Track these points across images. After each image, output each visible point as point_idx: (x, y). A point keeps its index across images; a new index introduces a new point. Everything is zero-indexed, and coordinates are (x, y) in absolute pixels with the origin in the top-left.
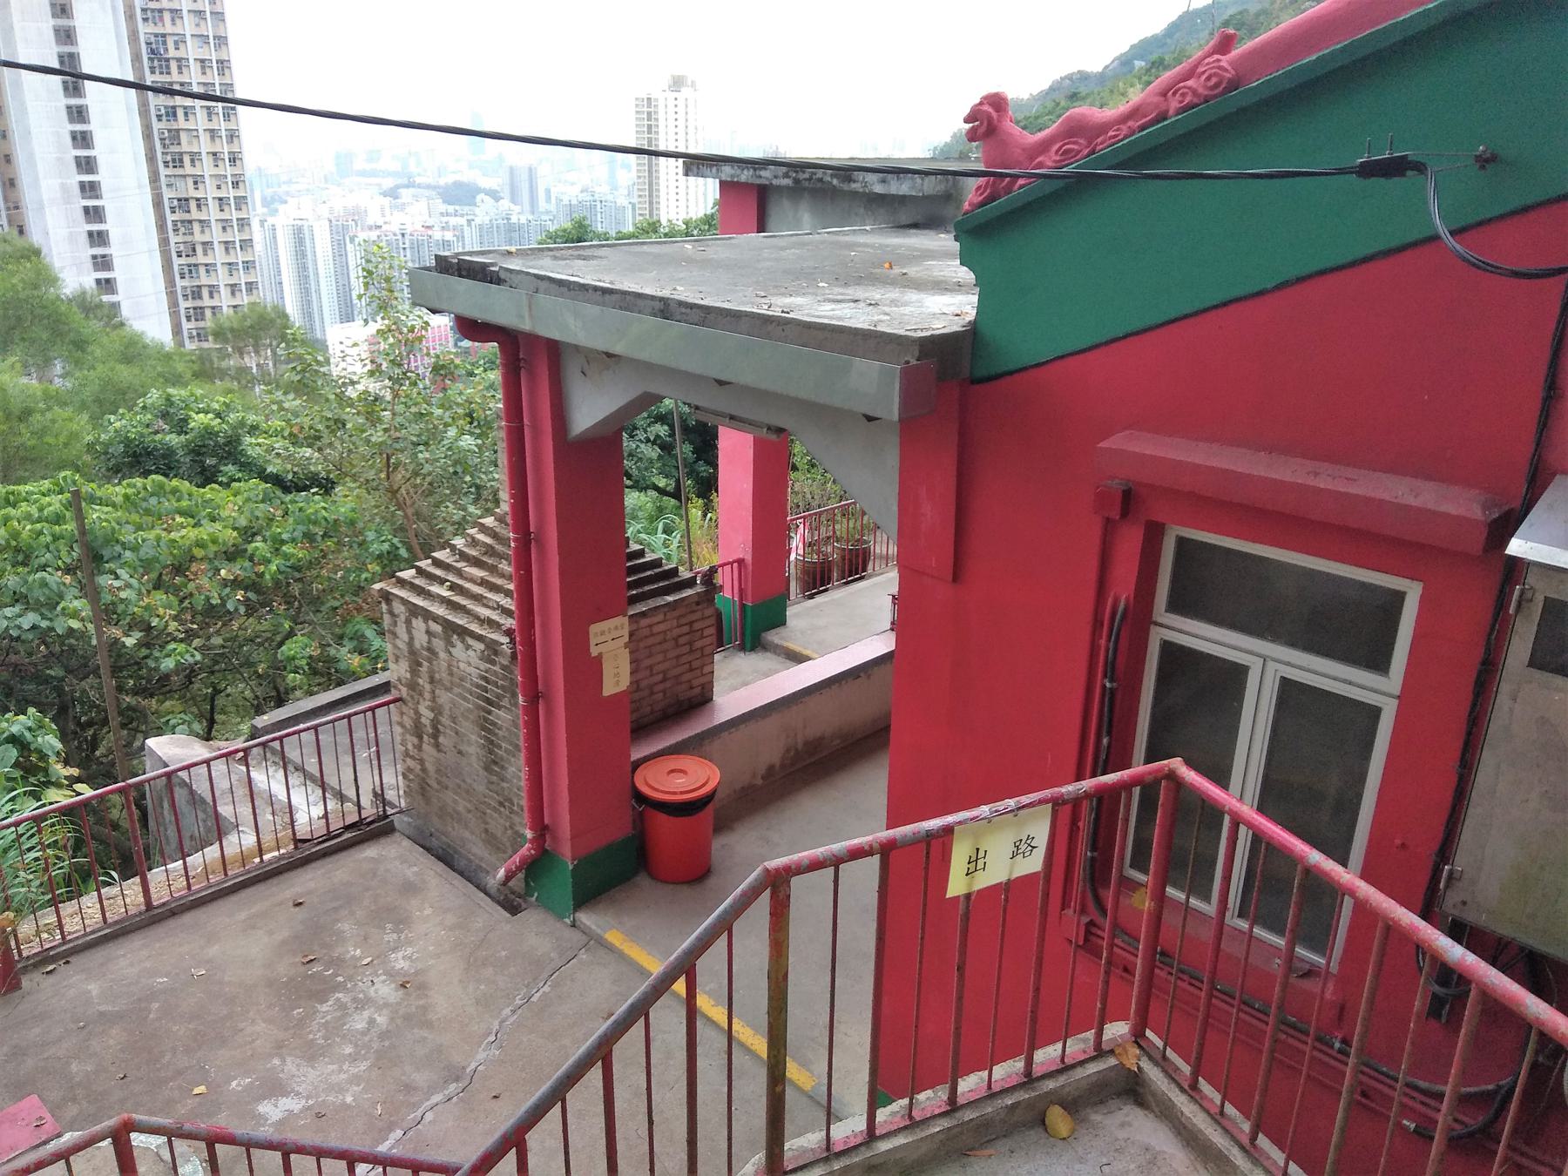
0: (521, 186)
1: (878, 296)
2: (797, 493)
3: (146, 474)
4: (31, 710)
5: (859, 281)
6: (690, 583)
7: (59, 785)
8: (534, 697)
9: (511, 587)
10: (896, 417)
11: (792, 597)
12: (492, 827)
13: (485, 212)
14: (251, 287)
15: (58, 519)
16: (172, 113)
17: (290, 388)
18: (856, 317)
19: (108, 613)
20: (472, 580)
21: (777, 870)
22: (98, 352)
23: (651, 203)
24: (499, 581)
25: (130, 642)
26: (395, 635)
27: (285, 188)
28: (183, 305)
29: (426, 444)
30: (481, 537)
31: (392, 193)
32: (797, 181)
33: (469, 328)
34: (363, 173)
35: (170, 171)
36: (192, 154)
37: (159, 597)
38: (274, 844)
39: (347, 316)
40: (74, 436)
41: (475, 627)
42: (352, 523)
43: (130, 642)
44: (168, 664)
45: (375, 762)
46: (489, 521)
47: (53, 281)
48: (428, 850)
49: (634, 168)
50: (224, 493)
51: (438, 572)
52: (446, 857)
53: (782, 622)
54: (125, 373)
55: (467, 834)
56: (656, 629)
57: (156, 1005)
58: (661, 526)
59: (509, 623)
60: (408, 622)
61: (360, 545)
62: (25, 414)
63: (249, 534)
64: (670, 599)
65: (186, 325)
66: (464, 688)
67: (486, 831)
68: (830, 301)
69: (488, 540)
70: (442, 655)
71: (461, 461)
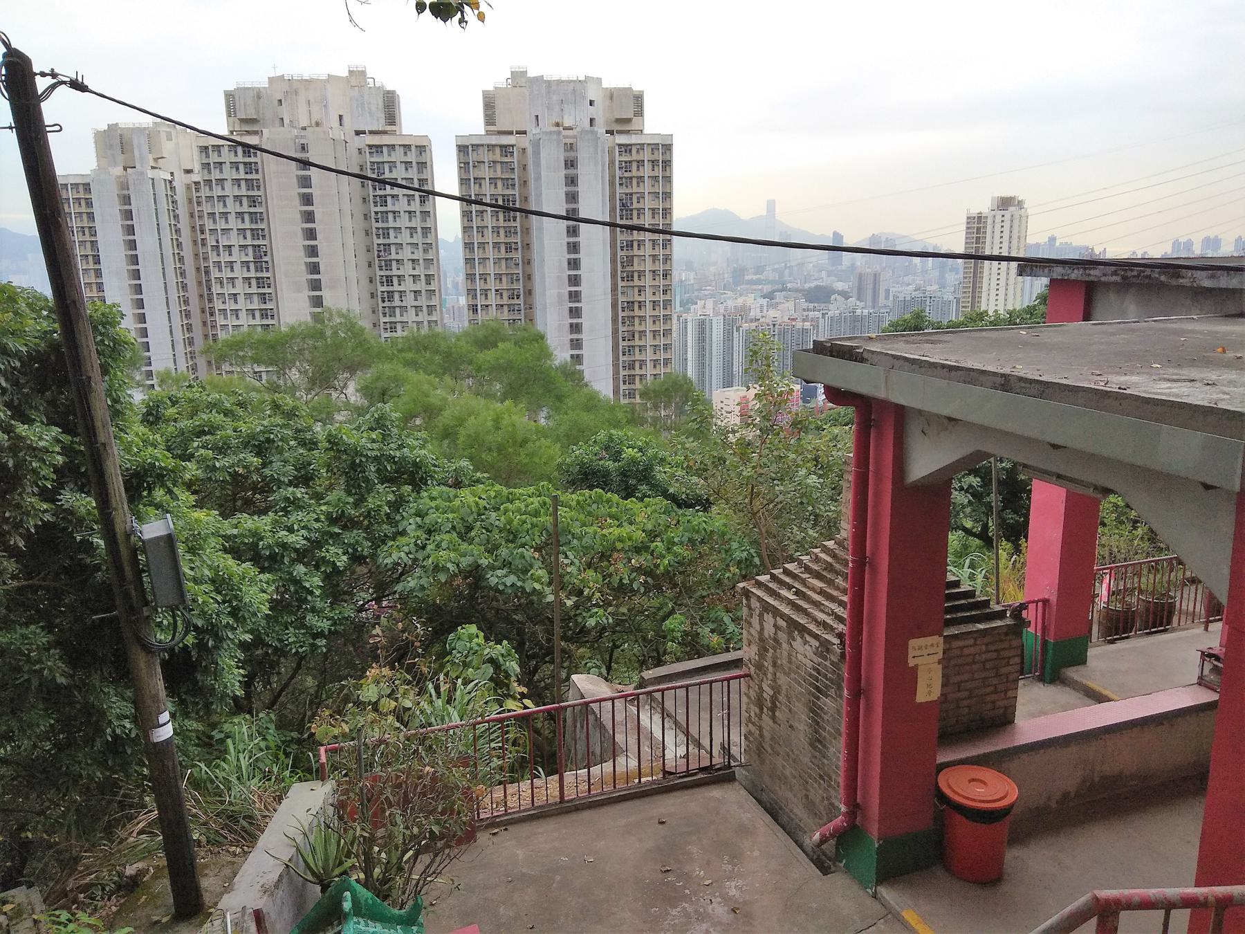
0: (867, 286)
1: (1214, 377)
2: (1104, 546)
3: (591, 488)
4: (505, 642)
5: (1193, 363)
6: (1000, 615)
7: (514, 698)
8: (858, 692)
9: (845, 598)
10: (1237, 488)
11: (1094, 639)
12: (812, 795)
13: (836, 308)
14: (667, 362)
15: (536, 514)
16: (630, 245)
17: (689, 434)
18: (1197, 396)
19: (558, 580)
20: (813, 589)
21: (1107, 901)
22: (570, 404)
23: (973, 297)
24: (835, 593)
25: (569, 603)
26: (750, 624)
27: (696, 293)
28: (622, 373)
29: (781, 480)
30: (823, 556)
31: (770, 296)
32: (1124, 278)
33: (835, 395)
34: (751, 282)
35: (624, 284)
36: (639, 272)
37: (591, 573)
38: (649, 770)
39: (728, 383)
40: (552, 458)
41: (812, 627)
42: (723, 534)
43: (569, 603)
44: (591, 622)
45: (726, 722)
46: (830, 544)
47: (549, 356)
48: (759, 801)
49: (961, 271)
50: (640, 505)
51: (787, 580)
52: (773, 811)
53: (1083, 661)
54: (586, 419)
55: (790, 795)
56: (966, 651)
57: (558, 878)
58: (968, 561)
59: (840, 627)
60: (761, 615)
61: (726, 551)
62: (524, 442)
63: (653, 535)
64: (981, 626)
65: (622, 387)
66: (800, 675)
67: (807, 797)
68: (1166, 380)
69: (829, 559)
70: (785, 646)
71: (805, 494)
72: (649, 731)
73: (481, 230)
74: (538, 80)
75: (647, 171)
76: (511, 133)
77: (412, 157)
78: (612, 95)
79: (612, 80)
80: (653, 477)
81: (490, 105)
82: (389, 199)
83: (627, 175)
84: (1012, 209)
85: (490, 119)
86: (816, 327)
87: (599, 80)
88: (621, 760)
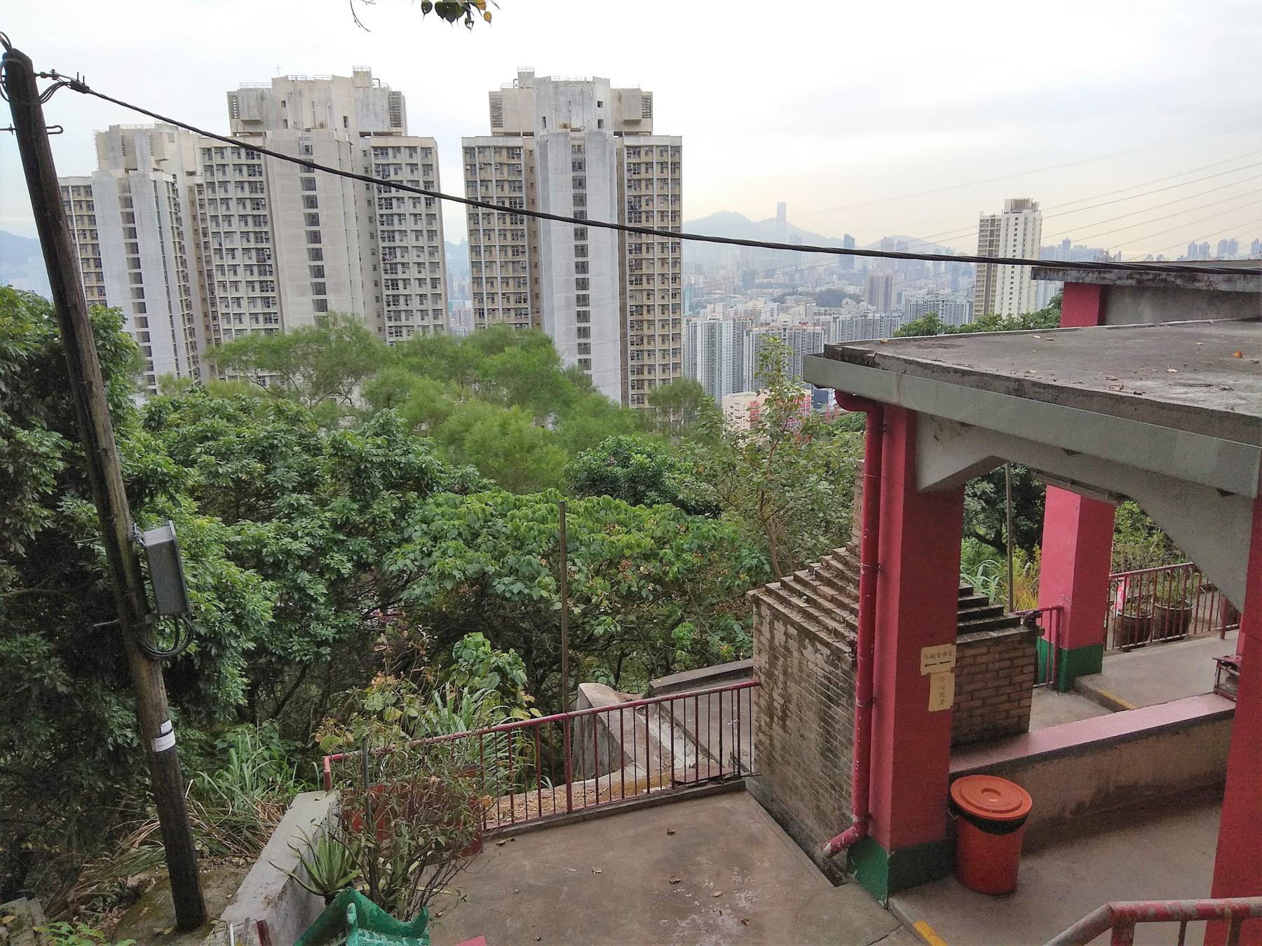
0: (878, 290)
1: (1231, 382)
2: (1119, 553)
3: (599, 494)
4: (512, 651)
5: (1209, 367)
6: (1014, 623)
7: (521, 707)
8: (870, 701)
9: (857, 606)
10: (1254, 494)
11: (1109, 648)
12: (823, 805)
13: (847, 311)
14: (676, 366)
15: (543, 520)
16: (638, 248)
17: (699, 439)
18: (1214, 401)
19: (565, 588)
20: (824, 597)
21: (1122, 913)
22: (578, 409)
23: (987, 301)
24: (846, 601)
25: (577, 611)
26: (760, 632)
27: (706, 297)
28: (631, 378)
29: (792, 486)
30: (834, 563)
31: (780, 300)
32: (1140, 281)
33: (846, 400)
34: (761, 286)
35: (632, 288)
36: (648, 275)
37: (599, 580)
38: (657, 780)
39: (738, 388)
40: (559, 464)
41: (823, 635)
42: (733, 541)
43: (577, 611)
44: (599, 630)
45: (736, 731)
46: (842, 551)
47: (556, 360)
48: (769, 811)
49: (975, 274)
50: (648, 511)
51: (798, 587)
52: (784, 822)
53: (1098, 670)
54: (594, 424)
55: (801, 805)
56: (979, 660)
57: (566, 889)
58: (981, 569)
59: (852, 636)
60: (771, 623)
61: (736, 558)
62: (532, 448)
63: (661, 542)
64: (994, 634)
65: (631, 392)
66: (811, 684)
67: (818, 807)
68: (1182, 385)
69: (840, 566)
70: (795, 654)
71: (816, 500)
72: (657, 741)
73: (487, 233)
74: (545, 81)
75: (656, 173)
76: (518, 135)
77: (418, 159)
78: (620, 96)
79: (621, 82)
80: (662, 483)
81: (497, 106)
82: (394, 202)
83: (635, 177)
84: (1025, 211)
85: (496, 121)
86: (827, 331)
87: (607, 81)
88: (629, 770)
